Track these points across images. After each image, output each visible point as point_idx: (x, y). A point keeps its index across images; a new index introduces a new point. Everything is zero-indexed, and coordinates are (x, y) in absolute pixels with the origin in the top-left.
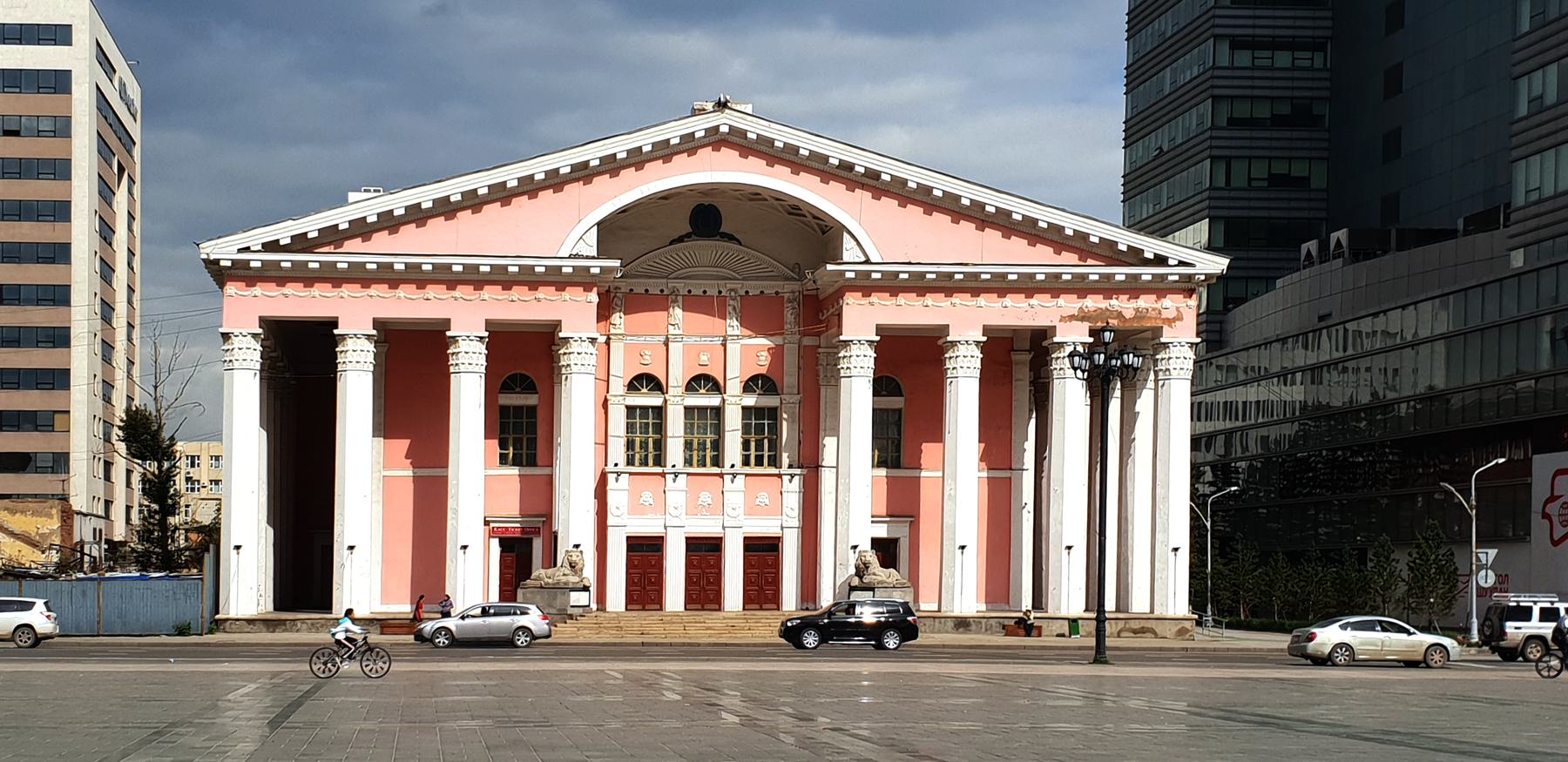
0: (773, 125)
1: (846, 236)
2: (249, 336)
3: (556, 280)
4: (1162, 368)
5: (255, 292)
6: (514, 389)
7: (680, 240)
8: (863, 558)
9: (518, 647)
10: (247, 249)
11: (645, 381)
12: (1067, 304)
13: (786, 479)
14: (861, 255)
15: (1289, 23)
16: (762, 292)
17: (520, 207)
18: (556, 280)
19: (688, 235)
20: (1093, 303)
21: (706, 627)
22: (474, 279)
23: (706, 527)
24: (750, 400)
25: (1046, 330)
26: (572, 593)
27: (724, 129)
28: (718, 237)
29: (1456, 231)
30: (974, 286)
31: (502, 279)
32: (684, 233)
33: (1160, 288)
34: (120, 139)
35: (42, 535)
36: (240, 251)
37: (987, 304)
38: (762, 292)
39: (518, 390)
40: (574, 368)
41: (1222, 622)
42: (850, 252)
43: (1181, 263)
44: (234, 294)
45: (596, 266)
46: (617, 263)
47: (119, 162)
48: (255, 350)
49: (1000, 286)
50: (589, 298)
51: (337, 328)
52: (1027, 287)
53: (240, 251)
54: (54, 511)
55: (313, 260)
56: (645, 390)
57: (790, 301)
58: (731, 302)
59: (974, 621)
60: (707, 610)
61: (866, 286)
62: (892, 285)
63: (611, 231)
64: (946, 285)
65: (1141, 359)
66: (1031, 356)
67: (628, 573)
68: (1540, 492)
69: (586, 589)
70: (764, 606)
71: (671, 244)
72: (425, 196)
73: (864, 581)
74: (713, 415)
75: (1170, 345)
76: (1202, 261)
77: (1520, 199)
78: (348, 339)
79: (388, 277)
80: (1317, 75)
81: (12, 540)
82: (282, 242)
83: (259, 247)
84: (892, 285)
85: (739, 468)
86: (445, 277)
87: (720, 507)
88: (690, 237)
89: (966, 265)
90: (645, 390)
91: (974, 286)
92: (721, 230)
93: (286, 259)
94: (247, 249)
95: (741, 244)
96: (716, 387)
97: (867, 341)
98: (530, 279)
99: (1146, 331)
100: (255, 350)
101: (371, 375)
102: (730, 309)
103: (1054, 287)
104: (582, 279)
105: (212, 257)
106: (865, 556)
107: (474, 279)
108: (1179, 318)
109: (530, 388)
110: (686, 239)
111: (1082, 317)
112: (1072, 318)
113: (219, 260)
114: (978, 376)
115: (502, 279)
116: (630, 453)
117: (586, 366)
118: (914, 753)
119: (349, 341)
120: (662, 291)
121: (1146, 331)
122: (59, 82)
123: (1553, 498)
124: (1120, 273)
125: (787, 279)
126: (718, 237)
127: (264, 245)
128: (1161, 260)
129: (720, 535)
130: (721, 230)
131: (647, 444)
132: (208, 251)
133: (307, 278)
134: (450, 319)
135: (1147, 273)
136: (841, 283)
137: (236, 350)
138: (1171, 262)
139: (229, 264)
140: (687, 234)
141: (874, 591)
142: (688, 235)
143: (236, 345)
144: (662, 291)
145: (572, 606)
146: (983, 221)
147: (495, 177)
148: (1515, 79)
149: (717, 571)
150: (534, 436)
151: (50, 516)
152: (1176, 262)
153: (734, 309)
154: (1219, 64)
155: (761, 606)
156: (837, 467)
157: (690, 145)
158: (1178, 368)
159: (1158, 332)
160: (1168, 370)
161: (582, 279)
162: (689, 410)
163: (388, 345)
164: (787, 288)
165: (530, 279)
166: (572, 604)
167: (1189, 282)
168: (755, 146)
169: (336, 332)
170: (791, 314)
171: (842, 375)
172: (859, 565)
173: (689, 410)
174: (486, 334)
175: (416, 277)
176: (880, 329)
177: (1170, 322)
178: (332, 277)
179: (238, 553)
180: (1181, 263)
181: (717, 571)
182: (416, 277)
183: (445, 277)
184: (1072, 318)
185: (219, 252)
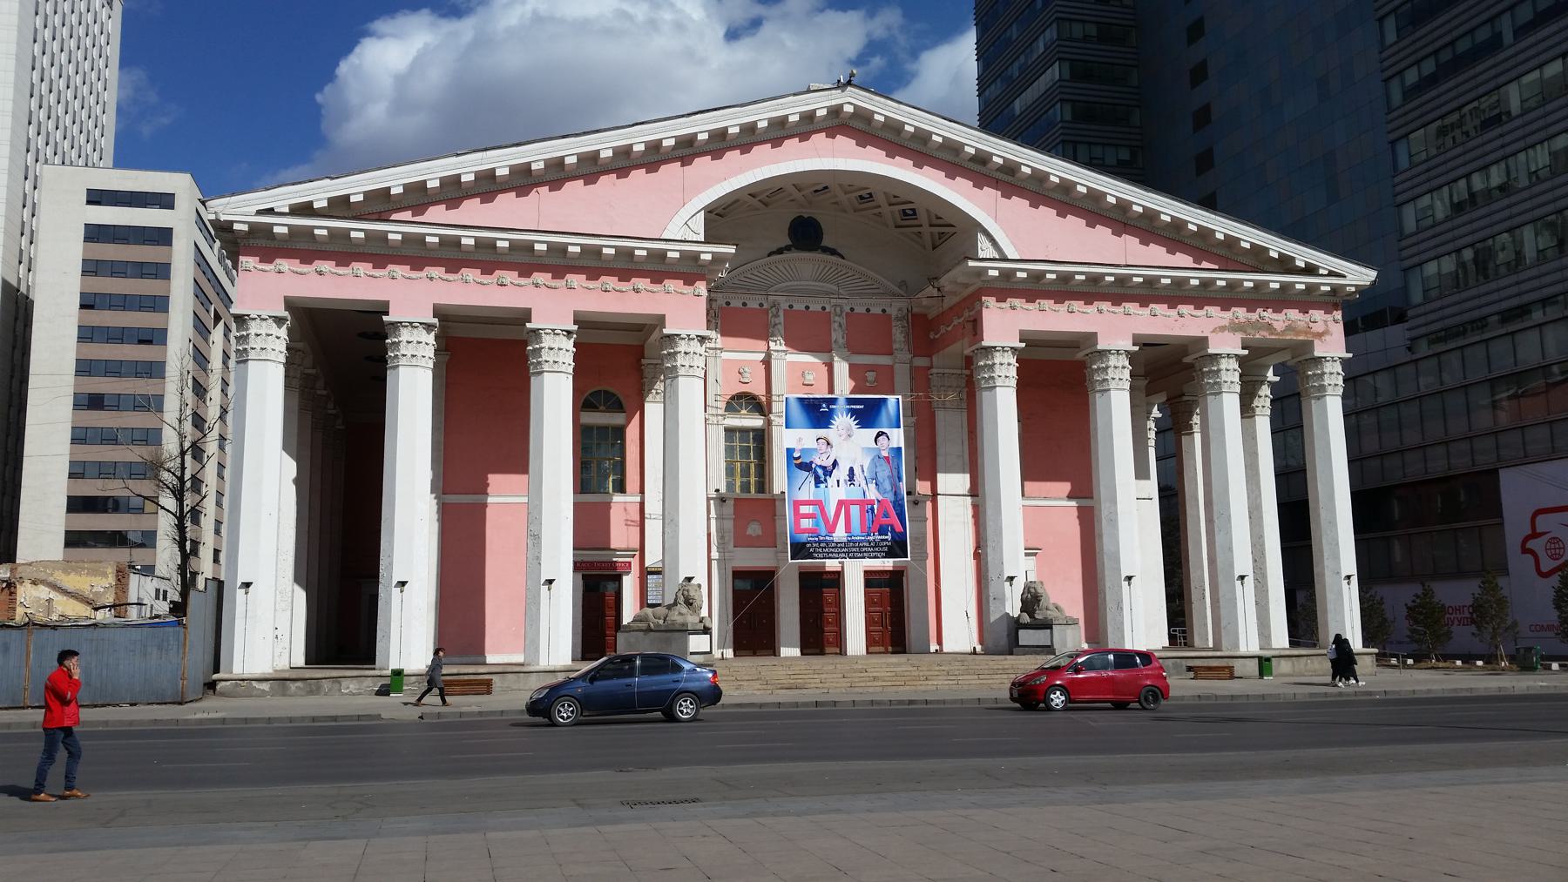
0: (902, 107)
1: (981, 237)
2: (270, 321)
3: (658, 268)
7: (780, 251)
8: (1033, 590)
9: (678, 720)
10: (270, 211)
11: (744, 401)
18: (658, 268)
22: (558, 263)
26: (691, 636)
27: (849, 109)
28: (820, 251)
30: (1121, 292)
31: (593, 264)
32: (783, 246)
33: (1308, 301)
34: (218, 294)
35: (97, 593)
36: (259, 213)
37: (1135, 312)
39: (602, 408)
41: (1398, 655)
42: (985, 249)
43: (1331, 274)
45: (707, 252)
46: (731, 250)
47: (215, 309)
48: (278, 338)
49: (1150, 293)
50: (697, 291)
51: (387, 313)
52: (1177, 295)
53: (259, 213)
54: (109, 570)
55: (358, 230)
56: (744, 412)
57: (898, 319)
58: (837, 318)
59: (1175, 666)
61: (1008, 288)
62: (1035, 288)
63: (720, 218)
64: (1093, 290)
66: (1147, 381)
68: (1515, 525)
69: (706, 631)
71: (769, 255)
72: (501, 161)
73: (1037, 616)
76: (1354, 273)
77: (1417, 296)
79: (451, 256)
81: (65, 598)
82: (316, 206)
84: (1035, 288)
86: (523, 260)
90: (744, 412)
91: (1121, 292)
92: (822, 244)
93: (321, 227)
94: (270, 211)
95: (843, 258)
96: (758, 406)
97: (1012, 348)
98: (625, 266)
100: (278, 338)
101: (430, 374)
102: (836, 325)
103: (1203, 296)
104: (689, 270)
105: (223, 218)
107: (558, 263)
108: (1326, 332)
109: (617, 406)
111: (1235, 327)
112: (1222, 329)
113: (232, 222)
115: (593, 264)
117: (695, 368)
118: (1320, 880)
119: (1112, 357)
120: (761, 305)
122: (163, 236)
123: (1535, 535)
125: (894, 295)
126: (820, 251)
128: (1310, 270)
130: (822, 244)
133: (342, 252)
134: (531, 309)
135: (1300, 282)
136: (979, 284)
139: (245, 228)
140: (786, 246)
142: (788, 248)
143: (252, 331)
144: (761, 305)
145: (691, 653)
147: (586, 144)
148: (1398, 206)
149: (836, 610)
151: (105, 575)
152: (1326, 272)
153: (840, 326)
157: (808, 126)
159: (1308, 345)
161: (689, 270)
163: (449, 353)
164: (895, 308)
165: (625, 266)
166: (691, 651)
167: (1334, 296)
168: (880, 133)
169: (385, 318)
170: (902, 332)
174: (576, 327)
175: (486, 258)
176: (1024, 336)
177: (1320, 335)
178: (379, 254)
180: (1331, 274)
181: (836, 610)
182: (486, 258)
183: (523, 260)
184: (1222, 329)
185: (232, 211)
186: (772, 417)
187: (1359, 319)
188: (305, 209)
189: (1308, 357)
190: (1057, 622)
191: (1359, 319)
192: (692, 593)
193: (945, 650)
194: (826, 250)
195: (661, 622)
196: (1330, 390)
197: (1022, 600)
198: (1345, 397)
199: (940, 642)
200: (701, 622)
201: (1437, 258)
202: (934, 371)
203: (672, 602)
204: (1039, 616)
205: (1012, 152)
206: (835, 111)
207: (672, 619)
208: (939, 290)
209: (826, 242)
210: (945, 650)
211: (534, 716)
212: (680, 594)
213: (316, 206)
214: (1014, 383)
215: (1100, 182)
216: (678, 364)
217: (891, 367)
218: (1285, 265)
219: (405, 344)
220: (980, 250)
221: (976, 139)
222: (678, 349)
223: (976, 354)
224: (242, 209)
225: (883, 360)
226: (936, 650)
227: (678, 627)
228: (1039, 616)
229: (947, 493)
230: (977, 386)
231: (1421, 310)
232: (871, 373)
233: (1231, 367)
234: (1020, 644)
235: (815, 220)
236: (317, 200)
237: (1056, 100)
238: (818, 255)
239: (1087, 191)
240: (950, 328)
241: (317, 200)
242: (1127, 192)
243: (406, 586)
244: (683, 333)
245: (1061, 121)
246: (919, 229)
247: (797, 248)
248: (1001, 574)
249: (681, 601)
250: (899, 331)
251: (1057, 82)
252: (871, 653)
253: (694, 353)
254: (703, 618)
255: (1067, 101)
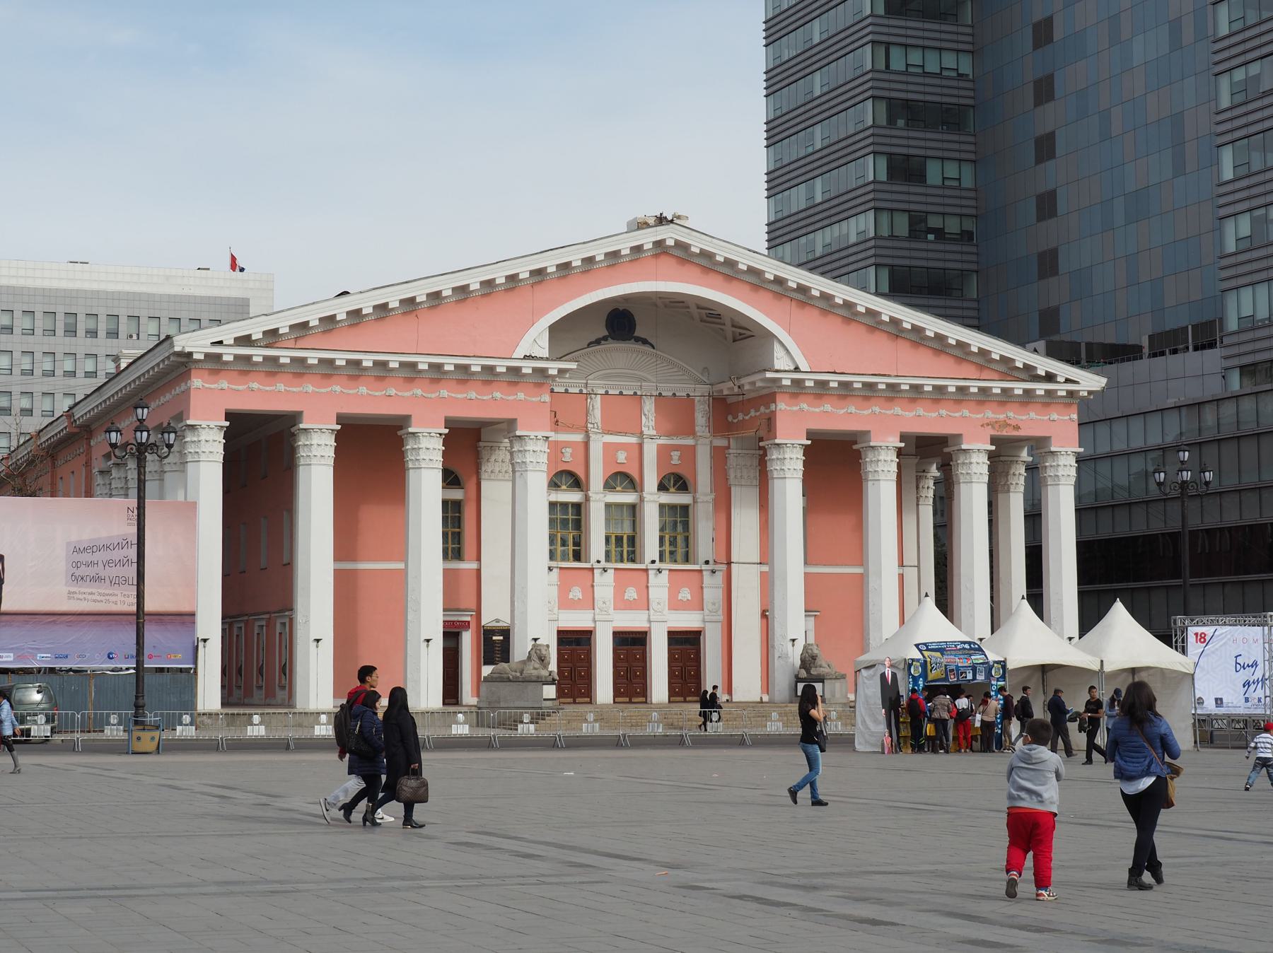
0: (714, 240)
1: (777, 347)
4: (1051, 474)
5: (223, 385)
6: (615, 488)
7: (598, 342)
8: (810, 651)
12: (1037, 417)
13: (651, 573)
14: (790, 364)
15: (939, 145)
16: (674, 394)
17: (477, 308)
19: (605, 338)
20: (990, 414)
21: (628, 719)
23: (632, 621)
24: (667, 498)
25: (947, 437)
26: (545, 687)
28: (633, 340)
29: (1139, 348)
32: (601, 336)
38: (674, 394)
40: (530, 468)
43: (1068, 381)
44: (201, 387)
56: (564, 487)
60: (578, 703)
65: (1189, 472)
67: (615, 666)
70: (578, 700)
73: (812, 672)
74: (575, 511)
75: (1059, 453)
77: (1232, 325)
78: (200, 430)
80: (964, 194)
83: (232, 342)
85: (603, 564)
87: (590, 602)
88: (607, 340)
89: (889, 376)
92: (636, 334)
94: (220, 343)
95: (654, 348)
96: (577, 483)
99: (503, 422)
105: (187, 350)
106: (540, 650)
110: (603, 342)
114: (332, 463)
116: (619, 549)
119: (883, 452)
121: (503, 422)
124: (1018, 388)
127: (236, 339)
128: (1050, 377)
129: (591, 629)
130: (636, 334)
131: (447, 534)
132: (183, 343)
135: (1040, 388)
137: (203, 443)
138: (1059, 379)
141: (823, 682)
142: (605, 338)
143: (203, 438)
145: (545, 700)
146: (897, 336)
150: (401, 566)
154: (878, 178)
155: (685, 699)
156: (918, 567)
158: (207, 451)
160: (1058, 476)
162: (608, 506)
171: (410, 466)
172: (805, 657)
173: (608, 506)
179: (317, 647)
180: (1068, 381)
186: (590, 493)
187: (1190, 327)
188: (245, 340)
189: (1047, 450)
190: (828, 677)
191: (1190, 327)
192: (544, 652)
193: (735, 699)
194: (638, 340)
195: (518, 674)
196: (1063, 481)
197: (801, 659)
198: (1078, 486)
199: (730, 692)
200: (550, 675)
201: (1252, 284)
202: (731, 451)
203: (525, 658)
204: (814, 672)
205: (804, 278)
206: (659, 244)
207: (529, 672)
208: (739, 387)
209: (639, 332)
210: (735, 699)
211: (1099, 726)
212: (533, 652)
213: (254, 338)
214: (800, 475)
215: (876, 304)
216: (528, 460)
217: (694, 447)
218: (1029, 373)
219: (315, 446)
220: (775, 359)
221: (775, 267)
222: (527, 448)
223: (770, 448)
224: (197, 343)
225: (689, 441)
226: (727, 700)
227: (534, 679)
228: (814, 672)
229: (741, 561)
230: (769, 476)
231: (1235, 339)
232: (676, 453)
233: (980, 461)
234: (798, 684)
235: (630, 312)
236: (255, 333)
237: (865, 40)
238: (631, 346)
239: (866, 311)
240: (747, 418)
241: (255, 333)
242: (898, 311)
243: (320, 643)
244: (532, 434)
245: (872, 15)
246: (722, 327)
247: (613, 339)
248: (784, 637)
249: (534, 657)
250: (701, 415)
251: (867, 17)
252: (673, 702)
253: (541, 451)
254: (551, 672)
255: (881, 42)
